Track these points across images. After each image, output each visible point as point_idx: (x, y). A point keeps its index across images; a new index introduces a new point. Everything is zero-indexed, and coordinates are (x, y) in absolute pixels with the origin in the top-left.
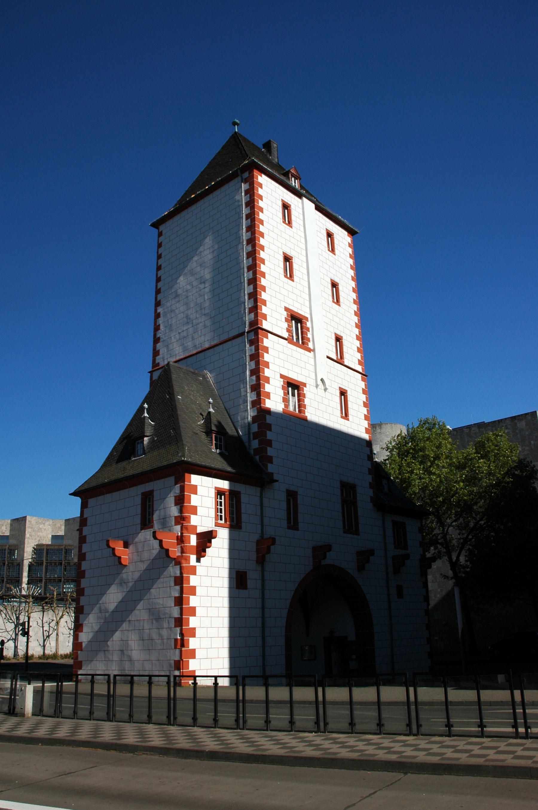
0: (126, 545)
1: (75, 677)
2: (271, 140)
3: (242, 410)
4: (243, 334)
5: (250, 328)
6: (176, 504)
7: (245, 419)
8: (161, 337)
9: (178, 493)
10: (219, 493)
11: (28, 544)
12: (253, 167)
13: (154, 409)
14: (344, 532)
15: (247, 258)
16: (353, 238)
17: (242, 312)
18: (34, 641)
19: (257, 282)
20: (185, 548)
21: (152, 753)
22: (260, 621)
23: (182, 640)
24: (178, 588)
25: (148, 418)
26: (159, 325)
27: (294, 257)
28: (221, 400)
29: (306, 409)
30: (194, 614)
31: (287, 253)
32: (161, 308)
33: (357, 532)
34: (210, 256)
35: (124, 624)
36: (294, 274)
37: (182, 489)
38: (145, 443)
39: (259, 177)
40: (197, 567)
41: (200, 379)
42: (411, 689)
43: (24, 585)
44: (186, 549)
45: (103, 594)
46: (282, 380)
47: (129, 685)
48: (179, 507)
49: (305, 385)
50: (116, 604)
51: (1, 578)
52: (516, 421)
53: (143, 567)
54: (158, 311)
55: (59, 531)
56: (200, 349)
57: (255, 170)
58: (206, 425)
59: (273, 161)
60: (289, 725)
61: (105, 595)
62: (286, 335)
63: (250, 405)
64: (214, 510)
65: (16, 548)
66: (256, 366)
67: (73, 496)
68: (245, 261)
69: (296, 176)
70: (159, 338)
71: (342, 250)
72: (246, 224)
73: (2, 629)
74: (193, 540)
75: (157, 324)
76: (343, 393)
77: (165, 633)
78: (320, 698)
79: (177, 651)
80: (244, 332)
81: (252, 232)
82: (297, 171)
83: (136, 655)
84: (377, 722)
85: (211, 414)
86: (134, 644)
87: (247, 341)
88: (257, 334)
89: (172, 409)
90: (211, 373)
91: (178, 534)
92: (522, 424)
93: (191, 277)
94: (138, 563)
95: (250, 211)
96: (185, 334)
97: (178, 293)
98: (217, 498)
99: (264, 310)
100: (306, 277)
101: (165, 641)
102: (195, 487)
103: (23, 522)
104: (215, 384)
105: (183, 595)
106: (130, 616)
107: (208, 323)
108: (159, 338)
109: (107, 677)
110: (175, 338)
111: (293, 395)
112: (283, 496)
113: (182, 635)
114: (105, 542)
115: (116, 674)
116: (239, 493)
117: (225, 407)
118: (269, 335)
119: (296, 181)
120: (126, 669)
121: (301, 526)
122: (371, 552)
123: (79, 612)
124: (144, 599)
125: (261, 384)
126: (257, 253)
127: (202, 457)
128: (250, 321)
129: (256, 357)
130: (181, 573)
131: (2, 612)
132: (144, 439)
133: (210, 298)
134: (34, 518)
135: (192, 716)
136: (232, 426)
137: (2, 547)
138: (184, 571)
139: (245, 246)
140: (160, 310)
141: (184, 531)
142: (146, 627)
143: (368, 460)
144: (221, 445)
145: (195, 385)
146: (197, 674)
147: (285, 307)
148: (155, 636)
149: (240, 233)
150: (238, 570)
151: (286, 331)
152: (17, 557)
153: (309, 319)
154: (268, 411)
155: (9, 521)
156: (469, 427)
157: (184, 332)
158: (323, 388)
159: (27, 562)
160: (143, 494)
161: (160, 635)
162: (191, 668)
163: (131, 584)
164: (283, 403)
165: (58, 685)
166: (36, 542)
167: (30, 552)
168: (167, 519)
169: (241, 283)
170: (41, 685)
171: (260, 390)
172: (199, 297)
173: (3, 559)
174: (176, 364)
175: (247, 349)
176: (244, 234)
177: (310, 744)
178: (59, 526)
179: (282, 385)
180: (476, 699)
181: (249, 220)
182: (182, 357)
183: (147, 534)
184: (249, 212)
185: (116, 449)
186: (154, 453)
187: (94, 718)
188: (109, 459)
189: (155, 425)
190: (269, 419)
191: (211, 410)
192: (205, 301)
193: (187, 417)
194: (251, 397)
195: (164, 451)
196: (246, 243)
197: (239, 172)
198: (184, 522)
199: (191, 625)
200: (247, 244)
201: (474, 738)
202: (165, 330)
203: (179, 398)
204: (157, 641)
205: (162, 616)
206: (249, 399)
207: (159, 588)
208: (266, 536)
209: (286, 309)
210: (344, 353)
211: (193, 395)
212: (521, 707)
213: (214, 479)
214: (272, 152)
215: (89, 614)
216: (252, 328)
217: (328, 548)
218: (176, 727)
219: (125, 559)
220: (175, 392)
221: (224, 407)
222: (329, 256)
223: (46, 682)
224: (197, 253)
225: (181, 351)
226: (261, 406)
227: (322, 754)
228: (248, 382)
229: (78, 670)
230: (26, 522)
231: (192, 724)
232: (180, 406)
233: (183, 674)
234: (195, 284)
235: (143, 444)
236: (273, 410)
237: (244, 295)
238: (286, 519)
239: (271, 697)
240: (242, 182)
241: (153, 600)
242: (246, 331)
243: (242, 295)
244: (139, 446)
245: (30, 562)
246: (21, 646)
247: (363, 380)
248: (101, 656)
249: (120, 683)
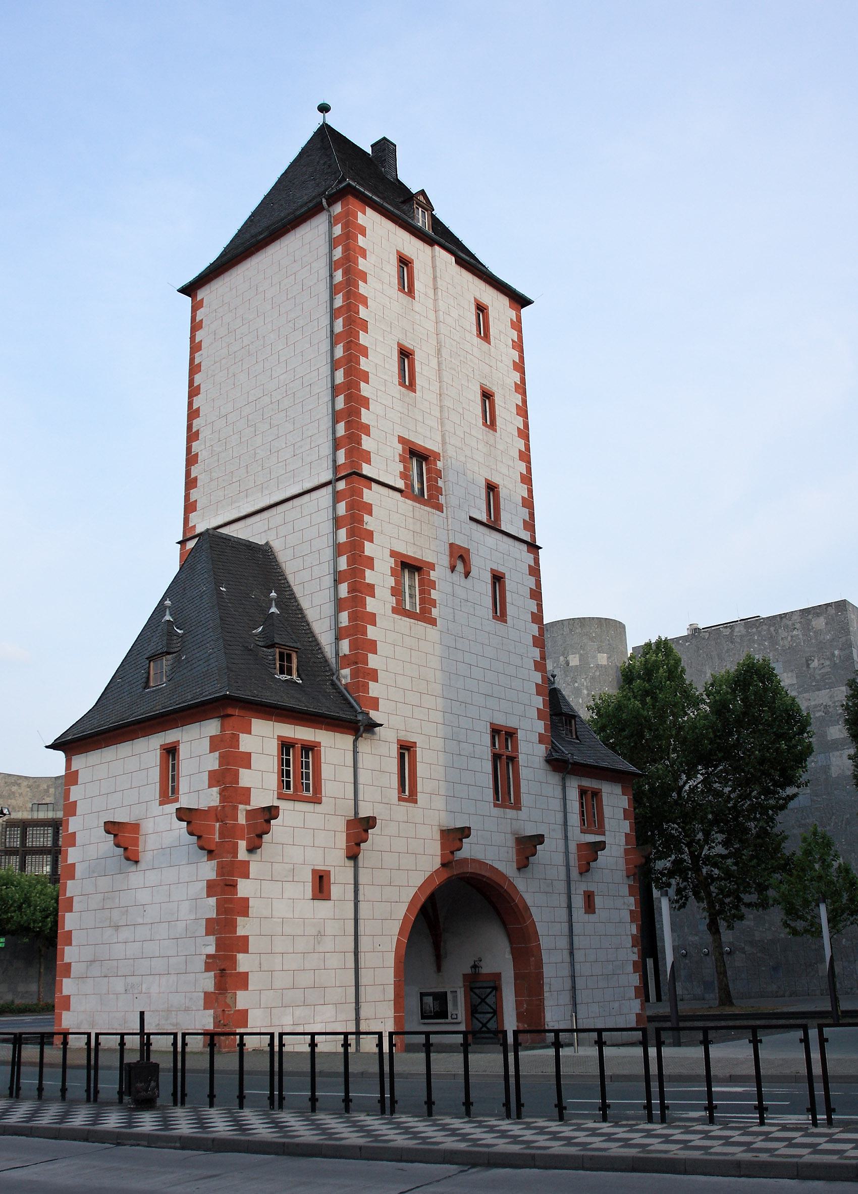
52: (810, 617)
55: (45, 797)
59: (389, 177)
62: (400, 484)
78: (817, 1070)
92: (819, 623)
118: (374, 485)
122: (539, 839)
178: (46, 788)
209: (402, 440)
217: (465, 832)
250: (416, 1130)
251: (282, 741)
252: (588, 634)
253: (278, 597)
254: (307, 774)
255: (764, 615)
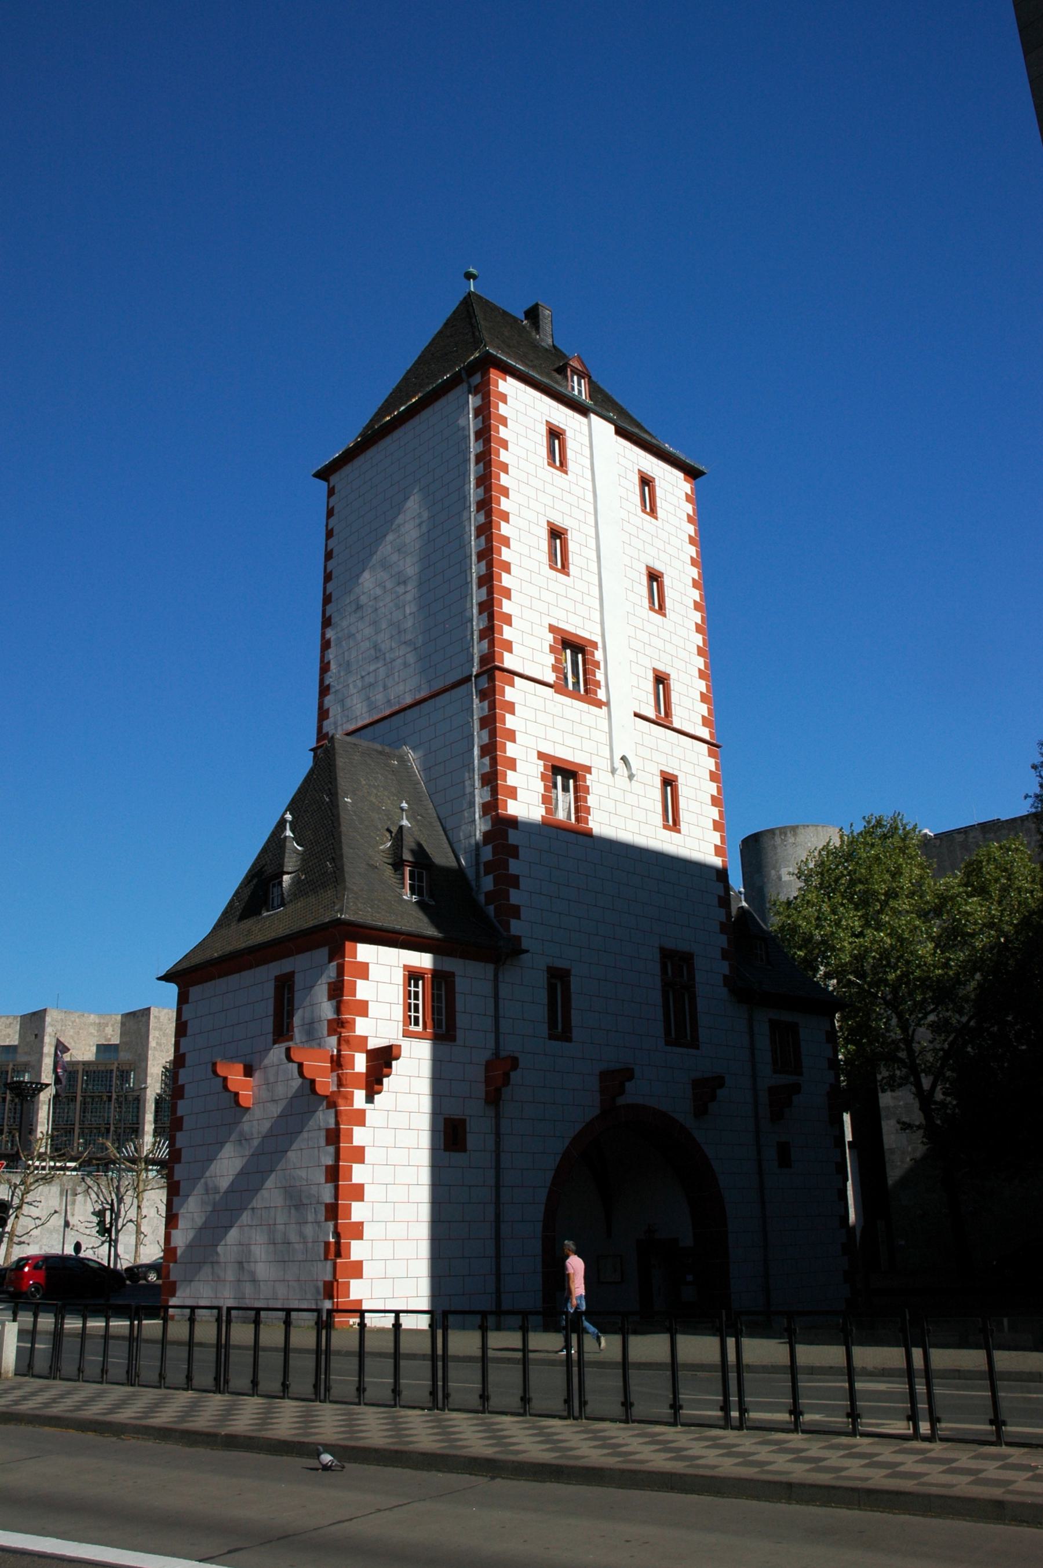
0: (249, 1072)
1: (162, 1310)
2: (539, 303)
3: (466, 821)
4: (467, 679)
5: (481, 668)
6: (330, 998)
7: (471, 836)
8: (332, 684)
9: (334, 978)
10: (413, 975)
11: (153, 1060)
12: (489, 363)
13: (303, 821)
14: (668, 1043)
15: (478, 536)
16: (695, 485)
17: (469, 637)
18: (150, 1244)
19: (493, 581)
20: (343, 1078)
21: (145, 1437)
22: (491, 1210)
23: (338, 1243)
24: (331, 1149)
25: (292, 840)
26: (329, 663)
27: (570, 529)
28: (432, 802)
29: (590, 815)
30: (360, 1198)
31: (556, 523)
32: (332, 630)
33: (694, 1044)
34: (415, 534)
35: (245, 1214)
36: (570, 561)
37: (341, 971)
38: (284, 886)
39: (501, 382)
40: (367, 1111)
41: (394, 764)
42: (731, 1342)
43: (148, 1139)
44: (346, 1079)
45: (211, 1160)
46: (541, 763)
47: (253, 1326)
48: (334, 1002)
49: (588, 769)
50: (231, 1178)
51: (105, 1124)
53: (276, 1110)
54: (328, 636)
56: (396, 708)
57: (492, 370)
58: (394, 850)
59: (543, 344)
60: (519, 1404)
61: (215, 1161)
62: (551, 677)
63: (479, 812)
64: (401, 1008)
65: (132, 1068)
66: (490, 739)
67: (164, 982)
68: (473, 543)
69: (582, 372)
70: (328, 686)
71: (671, 509)
72: (476, 472)
73: (90, 1222)
74: (360, 1063)
75: (326, 661)
76: (668, 782)
77: (309, 1230)
78: (732, 1357)
79: (329, 1264)
80: (471, 676)
81: (485, 487)
82: (582, 363)
83: (263, 1270)
84: (622, 1399)
85: (404, 831)
86: (260, 1251)
87: (476, 691)
88: (492, 679)
89: (333, 823)
90: (414, 751)
91: (333, 1051)
93: (382, 573)
94: (268, 1104)
95: (484, 447)
96: (371, 679)
97: (361, 603)
98: (407, 984)
99: (508, 633)
100: (594, 567)
101: (310, 1245)
102: (365, 966)
103: (144, 1019)
104: (421, 773)
105: (339, 1162)
106: (254, 1201)
107: (411, 658)
108: (328, 686)
109: (215, 1312)
110: (355, 686)
111: (565, 789)
112: (541, 979)
113: (337, 1235)
114: (210, 1066)
115: (229, 1305)
116: (452, 975)
117: (437, 814)
118: (517, 679)
119: (583, 381)
120: (247, 1296)
121: (575, 1033)
122: (719, 1081)
123: (174, 1191)
124: (277, 1169)
125: (499, 771)
126: (493, 527)
127: (380, 910)
128: (481, 654)
129: (490, 722)
130: (337, 1123)
131: (90, 1190)
132: (282, 878)
133: (414, 613)
134: (166, 1011)
135: (480, 1392)
136: (449, 850)
137: (97, 1067)
138: (343, 1118)
139: (473, 514)
140: (330, 634)
141: (344, 1047)
142: (280, 1220)
143: (720, 906)
144: (420, 888)
145: (382, 775)
146: (364, 1307)
147: (550, 625)
148: (293, 1237)
149: (466, 490)
150: (447, 1116)
151: (551, 669)
152: (134, 1085)
153: (600, 645)
154: (513, 822)
155: (119, 1018)
156: (965, 831)
157: (371, 674)
158: (626, 773)
159: (152, 1094)
160: (277, 979)
161: (301, 1234)
162: (354, 1295)
163: (256, 1143)
164: (543, 806)
165: (132, 1325)
166: (169, 1056)
167: (158, 1074)
168: (316, 1025)
169: (467, 584)
170: (104, 1324)
171: (497, 784)
172: (396, 610)
173: (108, 1088)
174: (348, 739)
175: (475, 706)
176: (472, 491)
177: (665, 1446)
179: (542, 772)
180: (787, 1361)
181: (481, 465)
182: (367, 721)
183: (277, 1053)
184: (482, 449)
185: (239, 895)
186: (299, 904)
187: (140, 1383)
188: (227, 915)
189: (304, 851)
190: (513, 837)
191: (405, 822)
192: (405, 617)
193: (358, 837)
194: (480, 796)
195: (314, 900)
196: (475, 508)
197: (464, 376)
198: (343, 1030)
199: (355, 1217)
200: (478, 511)
201: (843, 1437)
202: (339, 672)
203: (346, 802)
204: (297, 1246)
205: (305, 1201)
206: (478, 800)
207: (301, 1149)
208: (503, 1054)
209: (552, 629)
210: (673, 705)
211: (376, 794)
212: (924, 1380)
213: (402, 951)
214: (541, 326)
215: (188, 1196)
216: (485, 668)
217: (628, 1074)
218: (258, 1400)
219: (247, 1095)
220: (339, 791)
221: (435, 815)
222: (645, 522)
223: (88, 1319)
224: (394, 527)
225: (365, 710)
226: (498, 814)
227: (555, 1458)
228: (476, 769)
229: (170, 1298)
230: (149, 1019)
231: (251, 1392)
232: (345, 818)
233: (337, 1306)
234: (389, 585)
235: (282, 887)
236: (524, 819)
237: (470, 606)
238: (546, 1020)
239: (634, 1356)
240: (470, 392)
241: (292, 1170)
242: (474, 673)
243: (468, 607)
244: (275, 890)
245: (158, 1095)
246: (127, 1253)
247: (711, 754)
248: (207, 1270)
249: (236, 1323)
250: (606, 1434)
251: (409, 971)
252: (803, 844)
253: (353, 802)
254: (416, 1006)
255: (1003, 819)
